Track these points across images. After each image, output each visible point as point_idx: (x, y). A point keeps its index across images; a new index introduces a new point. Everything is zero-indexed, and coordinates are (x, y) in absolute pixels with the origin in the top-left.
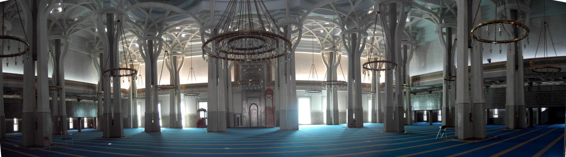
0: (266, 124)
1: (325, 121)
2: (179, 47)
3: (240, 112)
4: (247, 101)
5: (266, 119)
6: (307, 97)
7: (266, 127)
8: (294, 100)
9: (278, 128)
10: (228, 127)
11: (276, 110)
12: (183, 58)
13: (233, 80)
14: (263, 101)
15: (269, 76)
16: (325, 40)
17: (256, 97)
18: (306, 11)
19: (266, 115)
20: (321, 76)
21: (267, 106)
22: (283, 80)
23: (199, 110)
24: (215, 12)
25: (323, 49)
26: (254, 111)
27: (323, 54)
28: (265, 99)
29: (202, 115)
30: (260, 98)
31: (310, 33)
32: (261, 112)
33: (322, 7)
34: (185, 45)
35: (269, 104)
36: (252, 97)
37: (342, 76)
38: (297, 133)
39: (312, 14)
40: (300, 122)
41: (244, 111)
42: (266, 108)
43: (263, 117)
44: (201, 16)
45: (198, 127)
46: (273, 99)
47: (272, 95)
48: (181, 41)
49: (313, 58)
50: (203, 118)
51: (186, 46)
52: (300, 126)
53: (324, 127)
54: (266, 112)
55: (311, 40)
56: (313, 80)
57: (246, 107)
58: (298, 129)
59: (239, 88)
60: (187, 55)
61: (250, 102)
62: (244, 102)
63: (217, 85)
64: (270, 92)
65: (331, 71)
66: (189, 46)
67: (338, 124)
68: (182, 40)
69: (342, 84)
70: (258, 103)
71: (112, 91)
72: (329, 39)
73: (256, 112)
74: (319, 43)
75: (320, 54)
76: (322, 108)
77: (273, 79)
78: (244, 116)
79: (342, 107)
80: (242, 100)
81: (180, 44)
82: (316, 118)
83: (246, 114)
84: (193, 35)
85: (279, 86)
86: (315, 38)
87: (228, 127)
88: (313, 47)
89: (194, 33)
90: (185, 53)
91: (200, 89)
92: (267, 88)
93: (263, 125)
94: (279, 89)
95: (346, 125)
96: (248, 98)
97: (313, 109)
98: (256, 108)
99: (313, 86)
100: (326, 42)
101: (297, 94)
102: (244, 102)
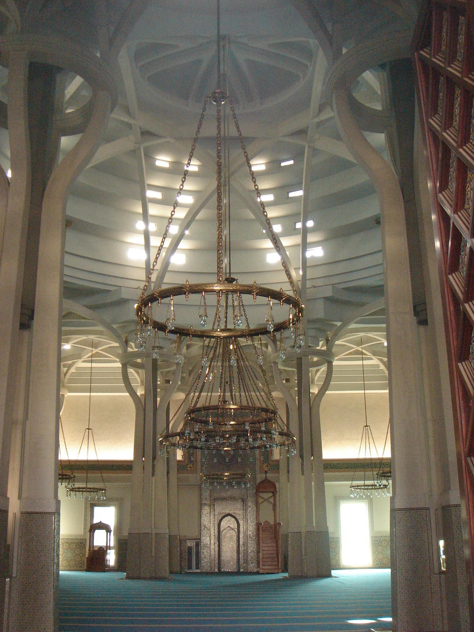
0: (258, 566)
3: (195, 534)
4: (212, 506)
5: (258, 552)
7: (258, 573)
8: (320, 504)
9: (286, 575)
10: (171, 572)
11: (282, 531)
14: (251, 504)
17: (233, 499)
18: (339, 324)
19: (258, 544)
21: (262, 521)
22: (296, 465)
23: (94, 527)
26: (225, 532)
28: (257, 505)
29: (100, 539)
30: (244, 501)
32: (246, 536)
33: (370, 315)
34: (69, 367)
35: (267, 516)
36: (224, 499)
39: (353, 326)
41: (204, 532)
42: (258, 525)
43: (252, 547)
44: (124, 327)
45: (88, 570)
46: (274, 506)
47: (274, 493)
50: (101, 548)
51: (73, 370)
54: (258, 535)
55: (360, 363)
56: (368, 456)
57: (208, 519)
59: (194, 478)
61: (221, 508)
62: (206, 510)
63: (153, 475)
64: (267, 487)
66: (77, 368)
70: (238, 512)
73: (234, 534)
74: (382, 367)
78: (206, 546)
80: (201, 505)
83: (208, 539)
84: (95, 351)
87: (171, 572)
89: (96, 348)
92: (260, 477)
93: (252, 567)
96: (214, 500)
98: (234, 525)
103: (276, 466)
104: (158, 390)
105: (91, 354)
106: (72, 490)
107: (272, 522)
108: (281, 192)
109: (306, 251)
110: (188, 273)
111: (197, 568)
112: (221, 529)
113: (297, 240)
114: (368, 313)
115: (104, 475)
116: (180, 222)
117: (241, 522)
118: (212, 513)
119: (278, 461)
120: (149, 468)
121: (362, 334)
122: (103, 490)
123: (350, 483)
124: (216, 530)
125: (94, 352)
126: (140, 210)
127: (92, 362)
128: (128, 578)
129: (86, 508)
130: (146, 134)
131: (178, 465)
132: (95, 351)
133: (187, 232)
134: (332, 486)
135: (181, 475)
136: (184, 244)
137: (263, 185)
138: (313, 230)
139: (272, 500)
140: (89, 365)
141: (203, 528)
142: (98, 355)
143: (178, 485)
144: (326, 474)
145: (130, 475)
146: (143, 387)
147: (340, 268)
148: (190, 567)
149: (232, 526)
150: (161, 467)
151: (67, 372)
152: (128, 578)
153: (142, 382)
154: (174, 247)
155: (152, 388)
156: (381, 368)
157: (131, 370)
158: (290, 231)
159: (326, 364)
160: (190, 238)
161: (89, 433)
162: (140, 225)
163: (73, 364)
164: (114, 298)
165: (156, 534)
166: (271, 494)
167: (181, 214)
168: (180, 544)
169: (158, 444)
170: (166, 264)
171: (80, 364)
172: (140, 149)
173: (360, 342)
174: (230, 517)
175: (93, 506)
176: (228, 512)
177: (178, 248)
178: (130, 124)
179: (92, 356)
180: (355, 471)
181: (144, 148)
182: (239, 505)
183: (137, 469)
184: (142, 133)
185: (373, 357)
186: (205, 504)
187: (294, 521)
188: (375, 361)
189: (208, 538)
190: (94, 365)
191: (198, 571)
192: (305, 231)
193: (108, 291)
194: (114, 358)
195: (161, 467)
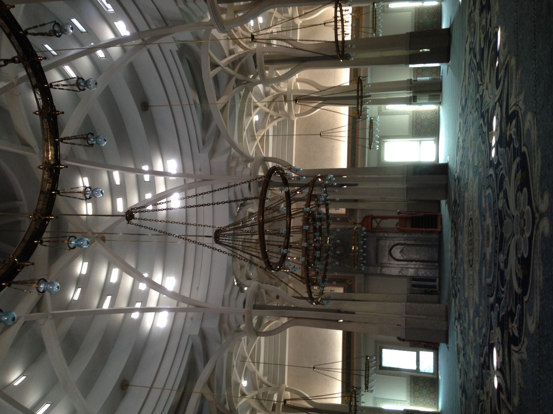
1: (432, 107)
2: (264, 394)
4: (382, 266)
6: (381, 145)
10: (439, 302)
12: (287, 389)
13: (340, 290)
15: (343, 219)
16: (272, 112)
17: (377, 248)
20: (342, 115)
24: (223, 305)
25: (288, 115)
27: (296, 115)
30: (378, 240)
31: (261, 141)
32: (407, 239)
34: (262, 382)
35: (392, 224)
37: (343, 76)
38: (453, 166)
40: (341, 398)
41: (405, 273)
47: (373, 218)
48: (255, 389)
49: (305, 135)
51: (265, 379)
52: (441, 161)
53: (445, 113)
55: (271, 138)
58: (445, 167)
59: (358, 280)
60: (283, 382)
61: (385, 259)
62: (386, 271)
64: (368, 219)
65: (334, 97)
66: (264, 375)
67: (441, 84)
68: (253, 386)
69: (356, 78)
70: (389, 243)
71: (421, 51)
72: (270, 103)
74: (275, 123)
75: (295, 119)
76: (404, 113)
77: (343, 211)
79: (404, 73)
81: (261, 391)
82: (426, 128)
84: (249, 359)
85: (356, 201)
86: (268, 131)
88: (283, 134)
89: (246, 358)
90: (276, 382)
91: (355, 355)
94: (362, 201)
95: (444, 67)
96: (378, 263)
97: (407, 131)
99: (361, 136)
100: (275, 110)
101: (374, 164)
102: (386, 271)
103: (350, 212)
104: (284, 305)
105: (252, 363)
106: (367, 387)
107: (397, 221)
108: (116, 191)
109: (170, 173)
110: (193, 276)
111: (434, 281)
112: (402, 258)
113: (160, 180)
114: (224, 123)
115: (360, 128)
116: (136, 281)
117: (396, 242)
118: (388, 265)
119: (347, 210)
120: (348, 317)
121: (245, 134)
122: (367, 359)
123: (367, 149)
124: (403, 263)
125: (250, 361)
126: (122, 315)
127: (258, 363)
128: (447, 342)
129: (383, 374)
130: (39, 306)
131: (348, 292)
132: (249, 359)
133: (146, 275)
134: (369, 162)
135: (356, 290)
136: (158, 278)
137: (107, 207)
138: (151, 165)
139: (378, 220)
140: (262, 366)
141: (400, 274)
142: (252, 357)
143: (365, 293)
144: (359, 166)
145: (355, 334)
146: (282, 318)
147: (186, 145)
148: (435, 287)
149: (399, 251)
150: (347, 306)
151: (267, 385)
152: (447, 342)
153: (277, 319)
154: (159, 288)
155: (280, 310)
156: (276, 124)
157: (266, 329)
158: (152, 185)
159: (266, 163)
160: (151, 273)
161: (320, 368)
162: (135, 315)
163: (259, 379)
164: (199, 341)
165: (406, 313)
166: (374, 221)
167: (129, 280)
168: (414, 293)
169: (319, 307)
170: (172, 295)
171: (261, 372)
172: (53, 315)
173: (253, 138)
174: (392, 251)
175: (381, 368)
176: (387, 252)
177: (160, 283)
178: (25, 322)
179: (254, 362)
180: (358, 145)
181: (54, 310)
182: (382, 243)
183: (350, 327)
184: (39, 311)
185: (266, 129)
186: (381, 271)
187: (394, 204)
188: (270, 128)
189: (410, 270)
190: (262, 360)
191: (437, 280)
192: (154, 173)
193: (192, 346)
194: (256, 343)
195: (347, 306)
